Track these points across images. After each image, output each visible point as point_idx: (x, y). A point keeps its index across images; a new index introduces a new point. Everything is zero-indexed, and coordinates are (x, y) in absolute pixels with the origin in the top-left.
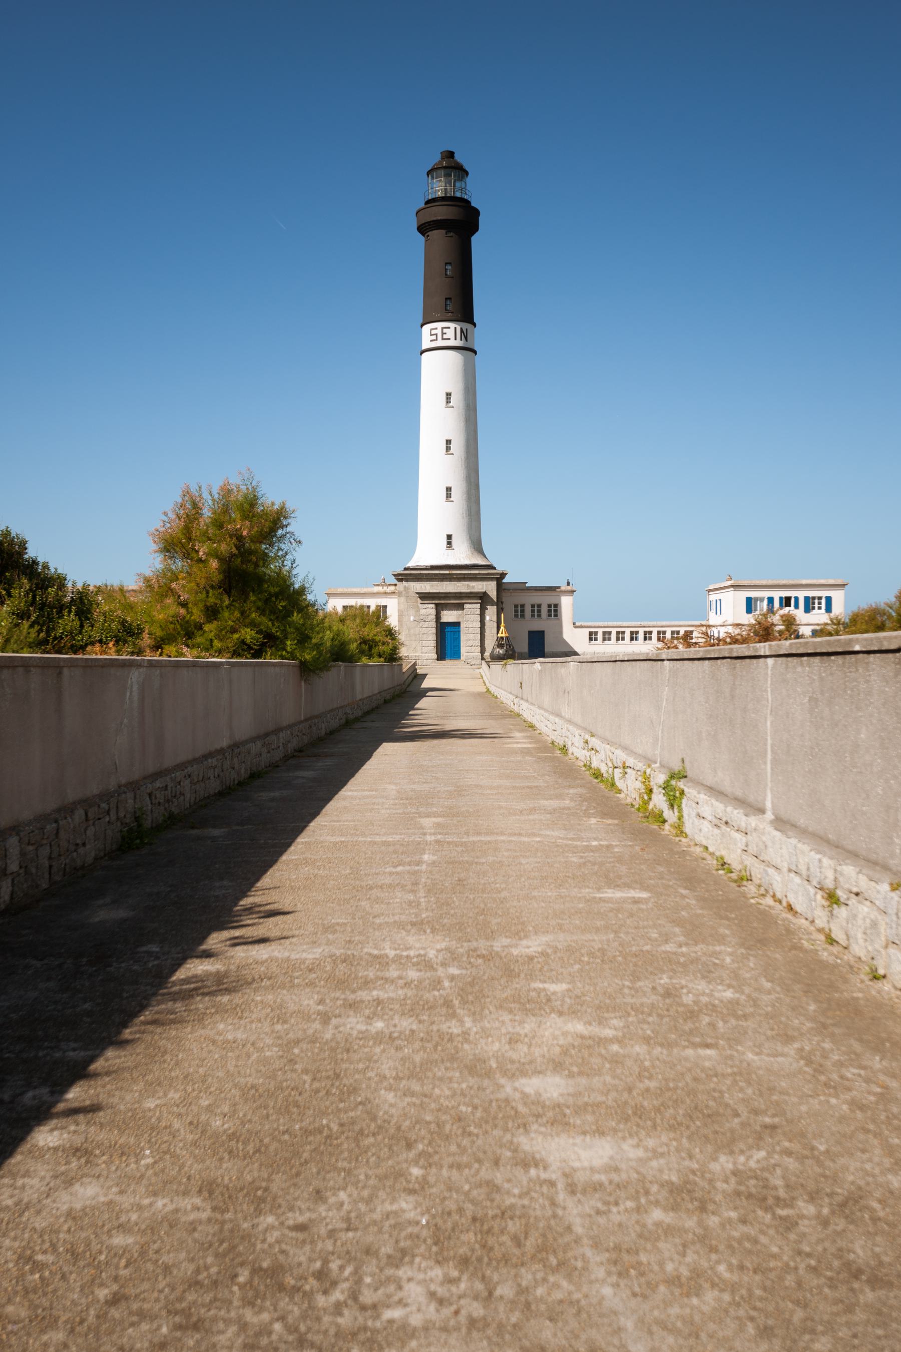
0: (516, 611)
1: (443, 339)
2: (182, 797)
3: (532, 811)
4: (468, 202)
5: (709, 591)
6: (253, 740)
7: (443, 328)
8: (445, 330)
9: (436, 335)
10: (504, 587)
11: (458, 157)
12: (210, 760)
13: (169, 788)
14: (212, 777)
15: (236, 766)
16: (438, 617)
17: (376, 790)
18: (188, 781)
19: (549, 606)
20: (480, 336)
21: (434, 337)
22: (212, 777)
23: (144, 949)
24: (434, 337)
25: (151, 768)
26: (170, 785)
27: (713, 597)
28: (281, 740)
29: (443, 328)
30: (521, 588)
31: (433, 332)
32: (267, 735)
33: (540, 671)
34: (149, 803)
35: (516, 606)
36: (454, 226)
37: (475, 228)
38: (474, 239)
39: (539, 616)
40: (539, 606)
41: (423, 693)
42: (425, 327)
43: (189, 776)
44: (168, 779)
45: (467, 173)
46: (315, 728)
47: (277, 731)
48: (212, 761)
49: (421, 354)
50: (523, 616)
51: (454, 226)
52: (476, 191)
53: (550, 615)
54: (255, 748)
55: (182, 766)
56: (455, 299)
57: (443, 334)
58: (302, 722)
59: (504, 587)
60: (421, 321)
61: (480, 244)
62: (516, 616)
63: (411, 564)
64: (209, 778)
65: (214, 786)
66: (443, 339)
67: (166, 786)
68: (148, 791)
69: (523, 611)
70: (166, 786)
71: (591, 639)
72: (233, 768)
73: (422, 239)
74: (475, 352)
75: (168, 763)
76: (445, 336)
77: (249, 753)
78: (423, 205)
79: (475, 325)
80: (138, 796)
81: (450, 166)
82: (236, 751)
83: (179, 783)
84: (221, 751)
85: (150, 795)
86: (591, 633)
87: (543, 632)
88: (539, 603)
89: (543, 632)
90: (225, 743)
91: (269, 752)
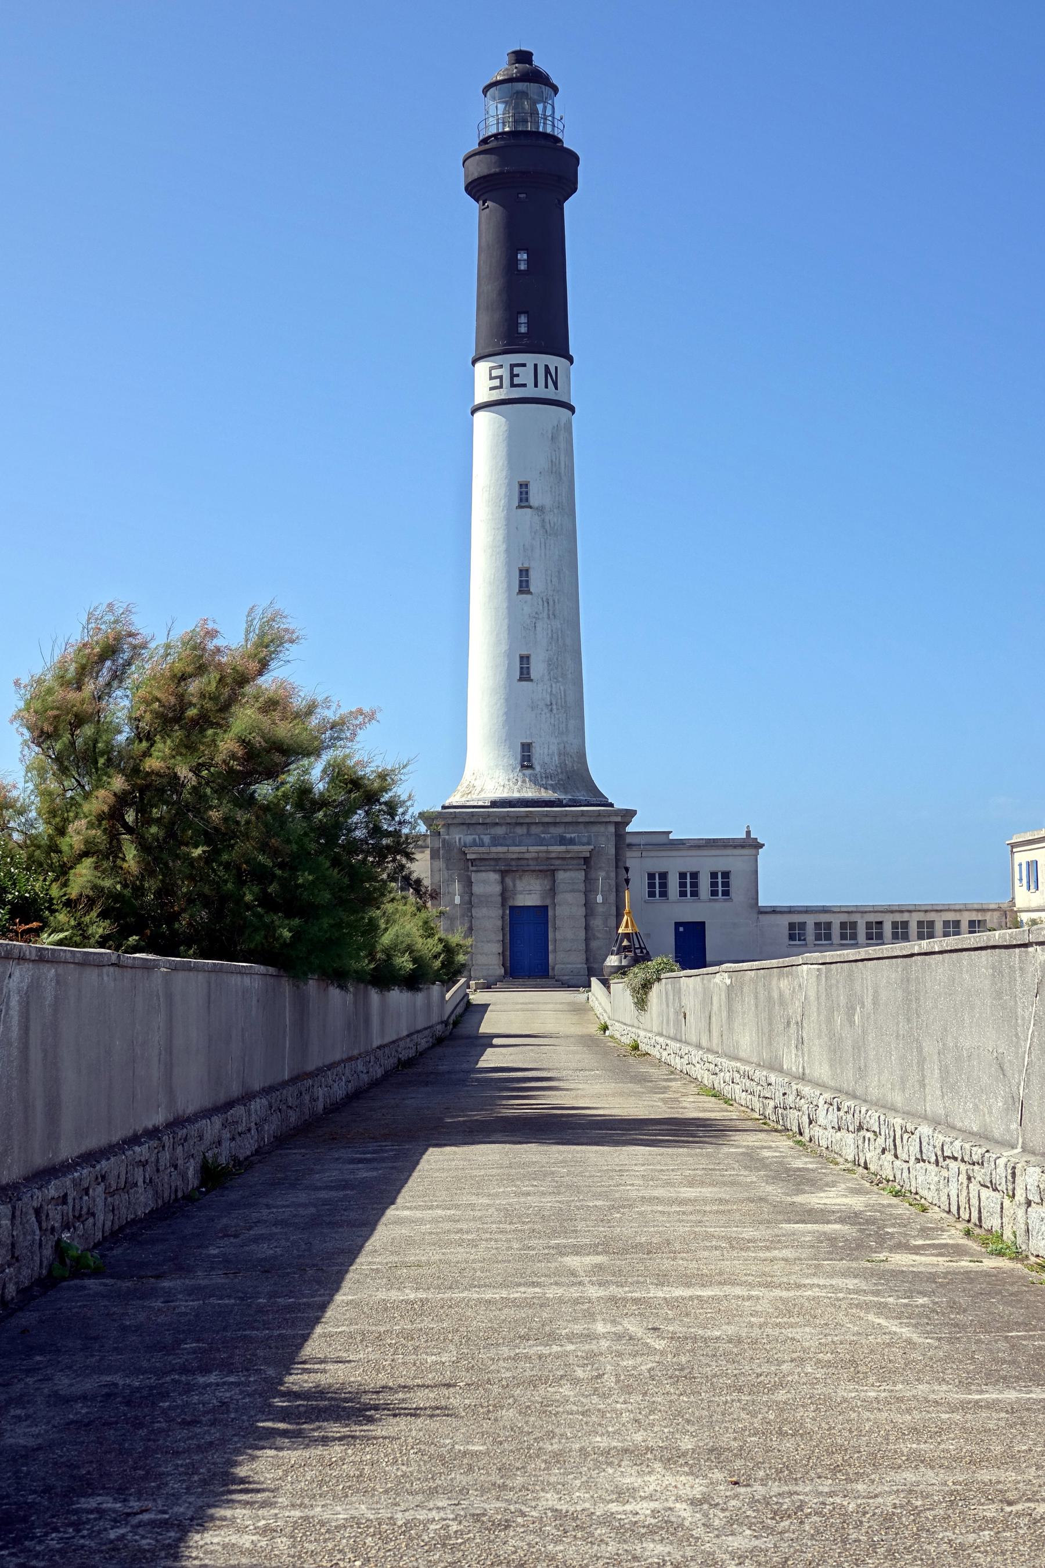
0: (651, 885)
1: (513, 385)
2: (91, 1220)
3: (775, 1242)
4: (558, 140)
5: (1013, 846)
6: (207, 1113)
7: (512, 366)
8: (516, 370)
9: (501, 378)
10: (629, 840)
11: (537, 61)
12: (137, 1149)
13: (70, 1200)
14: (140, 1183)
15: (180, 1162)
16: (505, 895)
17: (457, 1207)
18: (100, 1189)
19: (714, 875)
20: (581, 379)
21: (497, 382)
22: (140, 1183)
23: (92, 1503)
24: (497, 382)
25: (40, 1161)
26: (72, 1194)
27: (1022, 857)
28: (254, 1117)
29: (512, 366)
30: (662, 843)
31: (495, 373)
32: (230, 1105)
33: (730, 988)
34: (36, 1226)
35: (651, 876)
36: (525, 182)
37: (571, 188)
38: (569, 206)
39: (695, 894)
40: (695, 875)
41: (487, 1041)
42: (477, 365)
43: (103, 1178)
44: (67, 1181)
45: (555, 90)
46: (307, 1097)
47: (247, 1098)
48: (141, 1151)
49: (473, 413)
50: (664, 894)
51: (525, 182)
52: (569, 120)
53: (714, 893)
54: (212, 1127)
55: (89, 1158)
56: (528, 311)
57: (513, 376)
58: (284, 1084)
59: (629, 840)
60: (472, 354)
61: (584, 221)
62: (652, 894)
63: (455, 799)
64: (136, 1185)
65: (143, 1201)
66: (513, 385)
67: (65, 1195)
68: (35, 1204)
69: (664, 885)
70: (65, 1195)
71: (792, 937)
72: (176, 1167)
73: (474, 206)
74: (572, 409)
75: (67, 1150)
76: (516, 381)
77: (201, 1138)
78: (475, 146)
79: (571, 360)
80: (18, 1213)
81: (527, 77)
82: (182, 1133)
83: (86, 1191)
84: (153, 1133)
85: (38, 1212)
86: (792, 926)
87: (704, 923)
88: (694, 870)
89: (704, 923)
90: (158, 1118)
91: (233, 1139)
